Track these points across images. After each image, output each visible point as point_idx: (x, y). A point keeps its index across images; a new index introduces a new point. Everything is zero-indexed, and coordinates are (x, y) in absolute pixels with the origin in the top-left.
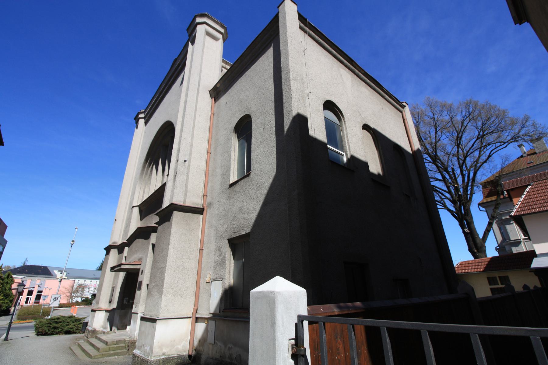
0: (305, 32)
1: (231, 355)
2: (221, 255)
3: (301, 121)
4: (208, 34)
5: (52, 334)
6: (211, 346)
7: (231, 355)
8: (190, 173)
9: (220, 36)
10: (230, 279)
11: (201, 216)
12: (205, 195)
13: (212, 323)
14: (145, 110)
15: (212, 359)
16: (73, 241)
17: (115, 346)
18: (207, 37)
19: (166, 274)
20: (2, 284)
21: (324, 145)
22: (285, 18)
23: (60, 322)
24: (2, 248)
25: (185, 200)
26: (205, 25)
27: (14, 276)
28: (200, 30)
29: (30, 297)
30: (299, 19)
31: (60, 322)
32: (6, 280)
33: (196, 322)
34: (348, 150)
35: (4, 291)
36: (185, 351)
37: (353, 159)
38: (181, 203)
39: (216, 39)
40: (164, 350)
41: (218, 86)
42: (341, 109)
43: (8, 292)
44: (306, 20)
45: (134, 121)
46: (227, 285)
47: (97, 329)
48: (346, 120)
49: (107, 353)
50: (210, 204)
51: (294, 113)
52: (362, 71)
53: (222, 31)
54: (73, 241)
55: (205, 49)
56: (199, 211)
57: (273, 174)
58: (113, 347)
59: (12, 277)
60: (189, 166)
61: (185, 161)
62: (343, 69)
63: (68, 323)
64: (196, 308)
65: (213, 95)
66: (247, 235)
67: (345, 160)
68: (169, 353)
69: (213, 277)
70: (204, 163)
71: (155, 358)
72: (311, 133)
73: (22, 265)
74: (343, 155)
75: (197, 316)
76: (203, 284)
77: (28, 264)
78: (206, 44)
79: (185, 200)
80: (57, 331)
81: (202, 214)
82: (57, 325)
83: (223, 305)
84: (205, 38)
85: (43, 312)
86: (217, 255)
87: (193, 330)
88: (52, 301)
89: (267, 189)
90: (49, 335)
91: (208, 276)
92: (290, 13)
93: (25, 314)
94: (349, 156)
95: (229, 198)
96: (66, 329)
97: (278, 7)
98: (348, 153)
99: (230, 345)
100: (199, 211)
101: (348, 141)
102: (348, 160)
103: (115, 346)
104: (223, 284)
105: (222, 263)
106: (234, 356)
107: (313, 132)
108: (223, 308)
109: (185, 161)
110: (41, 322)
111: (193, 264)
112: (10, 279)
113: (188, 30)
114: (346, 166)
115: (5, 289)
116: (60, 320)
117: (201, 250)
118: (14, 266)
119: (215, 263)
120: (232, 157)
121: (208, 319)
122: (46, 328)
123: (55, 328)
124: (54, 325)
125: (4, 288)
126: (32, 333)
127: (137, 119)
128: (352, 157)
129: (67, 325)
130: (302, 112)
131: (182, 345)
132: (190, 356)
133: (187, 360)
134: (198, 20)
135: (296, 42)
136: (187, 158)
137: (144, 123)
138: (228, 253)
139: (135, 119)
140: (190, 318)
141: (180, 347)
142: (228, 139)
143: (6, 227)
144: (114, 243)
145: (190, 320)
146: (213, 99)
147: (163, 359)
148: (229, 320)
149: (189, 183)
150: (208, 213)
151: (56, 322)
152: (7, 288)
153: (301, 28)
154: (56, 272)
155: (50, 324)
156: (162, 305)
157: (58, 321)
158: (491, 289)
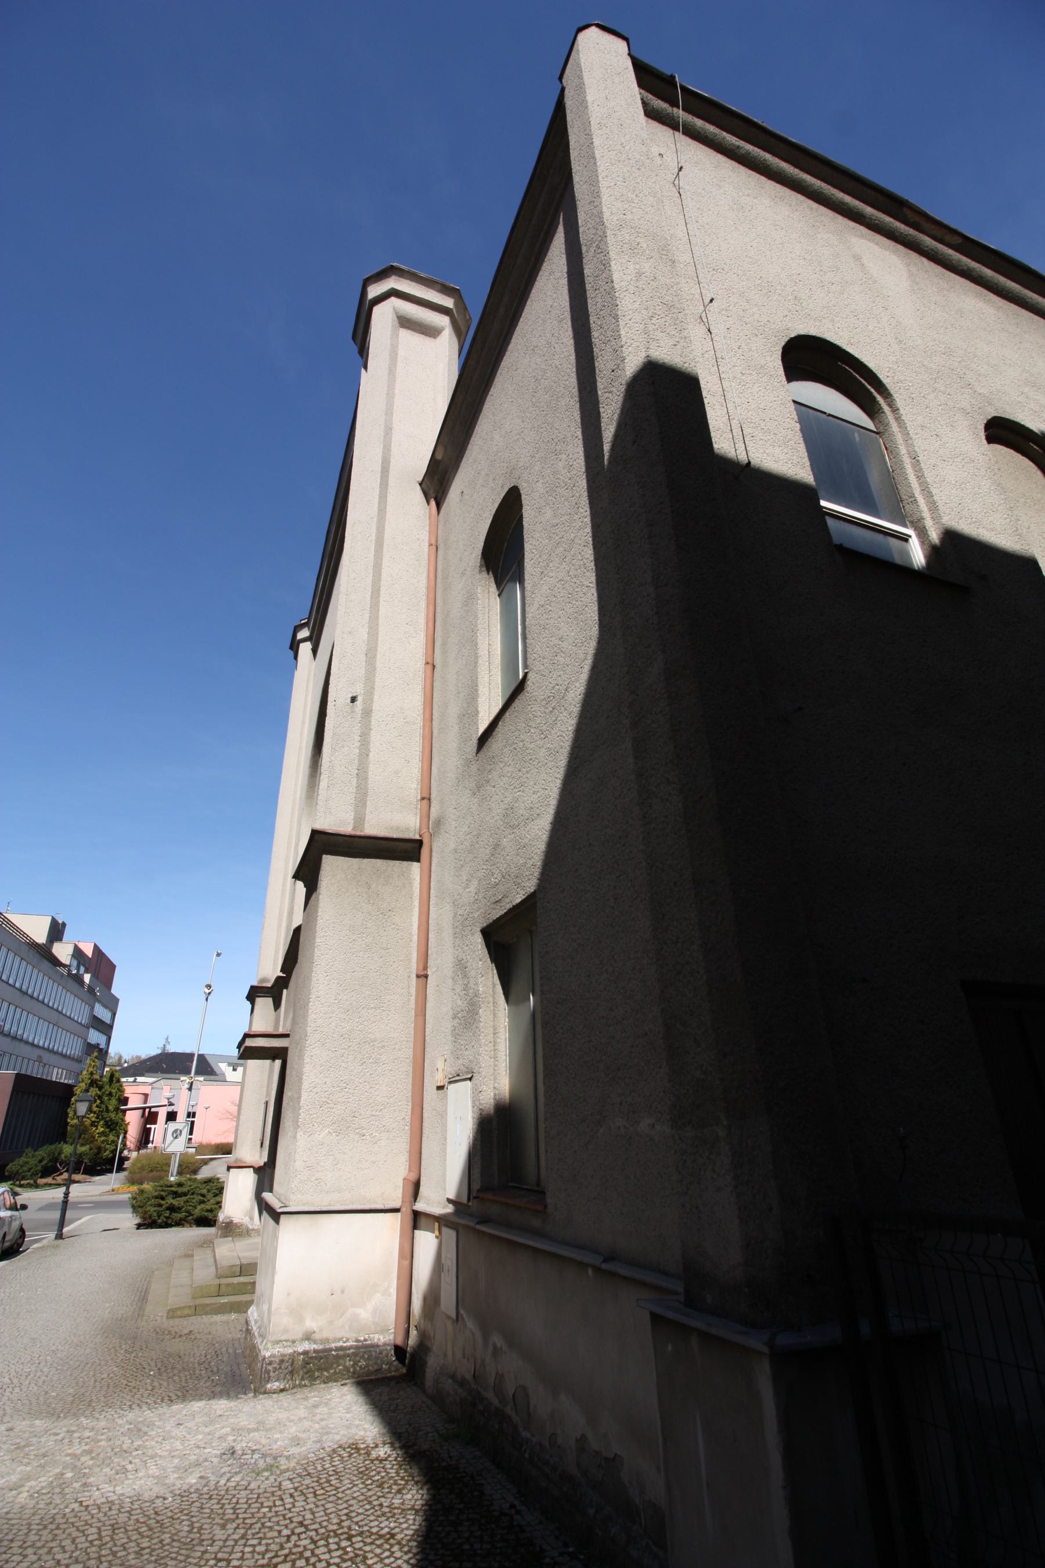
0: (671, 123)
1: (500, 1377)
2: (466, 987)
3: (668, 398)
4: (405, 322)
5: (166, 1225)
6: (449, 1323)
7: (500, 1377)
8: (373, 733)
9: (444, 321)
10: (498, 1077)
11: (415, 864)
12: (427, 799)
13: (450, 1234)
14: (309, 618)
15: (453, 1377)
16: (209, 986)
17: (236, 1280)
18: (405, 334)
19: (307, 1060)
20: (100, 1097)
21: (796, 497)
22: (583, 104)
23: (185, 1194)
24: (110, 1014)
25: (360, 820)
26: (393, 300)
27: (123, 1080)
28: (382, 317)
29: (153, 1127)
30: (640, 85)
31: (185, 1194)
32: (107, 1088)
33: (415, 1227)
34: (926, 513)
35: (105, 1115)
36: (384, 1331)
37: (955, 548)
38: (347, 829)
39: (431, 332)
40: (310, 1323)
41: (439, 457)
42: (871, 365)
43: (113, 1115)
44: (670, 81)
45: (291, 653)
46: (488, 1100)
47: (235, 1220)
48: (899, 402)
49: (208, 1301)
50: (439, 823)
51: (632, 365)
52: (948, 238)
53: (448, 302)
54: (209, 986)
55: (400, 365)
56: (405, 850)
57: (590, 647)
58: (228, 1285)
59: (118, 1081)
60: (367, 713)
61: (353, 699)
62: (862, 236)
63: (203, 1196)
64: (413, 1177)
65: (432, 493)
66: (530, 902)
67: (917, 556)
68: (325, 1335)
69: (451, 1070)
70: (416, 699)
71: (277, 1350)
72: (724, 442)
73: (159, 1052)
74: (905, 539)
75: (420, 1206)
76: (430, 1093)
77: (172, 1049)
78: (401, 352)
79: (360, 820)
80: (177, 1216)
81: (418, 860)
82: (176, 1202)
83: (477, 1173)
84: (395, 336)
85: (180, 1165)
86: (459, 988)
87: (408, 1254)
88: (169, 1138)
89: (576, 710)
90: (161, 1226)
91: (440, 1065)
92: (602, 70)
93: (142, 1168)
94: (935, 536)
95: (479, 787)
96: (197, 1212)
97: (561, 78)
98: (929, 523)
99: (497, 1339)
100: (405, 850)
101: (920, 477)
102: (934, 553)
103: (236, 1280)
104: (476, 1092)
105: (468, 1018)
106: (510, 1389)
107: (740, 446)
108: (476, 1186)
109: (353, 699)
110: (142, 1192)
111: (395, 1026)
112: (115, 1085)
113: (354, 338)
114: (926, 572)
115: (108, 1110)
116: (184, 1189)
117: (423, 976)
118: (137, 1057)
119: (455, 1017)
120: (483, 651)
121: (441, 1221)
122: (152, 1209)
123: (172, 1209)
124: (170, 1200)
125: (103, 1106)
126: (128, 1219)
127: (294, 646)
128: (951, 537)
129: (203, 1202)
130: (666, 353)
131: (370, 1306)
132: (399, 1351)
133: (390, 1363)
134: (374, 291)
135: (637, 171)
136: (359, 690)
137: (310, 653)
138: (487, 979)
139: (291, 648)
140: (396, 1210)
141: (364, 1314)
142: (470, 599)
143: (114, 967)
144: (263, 980)
145: (395, 1219)
146: (433, 503)
147: (305, 1353)
148: (492, 1236)
149: (371, 767)
150: (441, 851)
151: (176, 1195)
152: (111, 1108)
153: (651, 113)
154: (223, 1067)
155: (163, 1198)
156: (299, 1164)
157: (180, 1190)
158: (192, 1055)
